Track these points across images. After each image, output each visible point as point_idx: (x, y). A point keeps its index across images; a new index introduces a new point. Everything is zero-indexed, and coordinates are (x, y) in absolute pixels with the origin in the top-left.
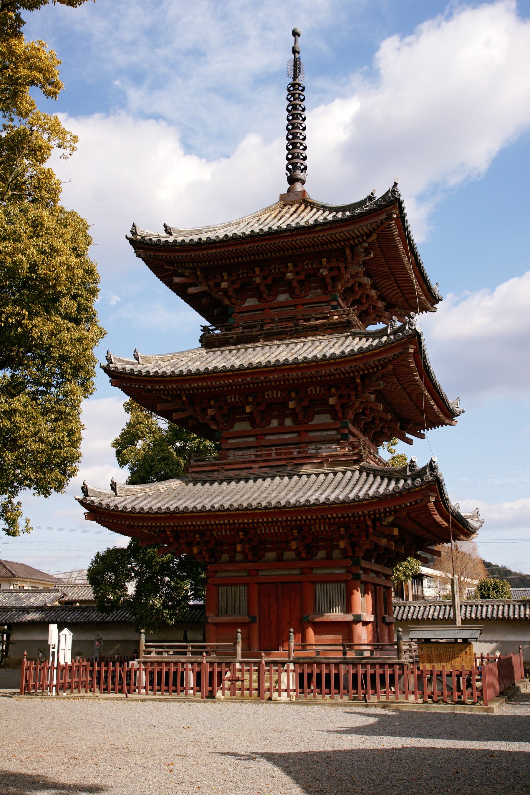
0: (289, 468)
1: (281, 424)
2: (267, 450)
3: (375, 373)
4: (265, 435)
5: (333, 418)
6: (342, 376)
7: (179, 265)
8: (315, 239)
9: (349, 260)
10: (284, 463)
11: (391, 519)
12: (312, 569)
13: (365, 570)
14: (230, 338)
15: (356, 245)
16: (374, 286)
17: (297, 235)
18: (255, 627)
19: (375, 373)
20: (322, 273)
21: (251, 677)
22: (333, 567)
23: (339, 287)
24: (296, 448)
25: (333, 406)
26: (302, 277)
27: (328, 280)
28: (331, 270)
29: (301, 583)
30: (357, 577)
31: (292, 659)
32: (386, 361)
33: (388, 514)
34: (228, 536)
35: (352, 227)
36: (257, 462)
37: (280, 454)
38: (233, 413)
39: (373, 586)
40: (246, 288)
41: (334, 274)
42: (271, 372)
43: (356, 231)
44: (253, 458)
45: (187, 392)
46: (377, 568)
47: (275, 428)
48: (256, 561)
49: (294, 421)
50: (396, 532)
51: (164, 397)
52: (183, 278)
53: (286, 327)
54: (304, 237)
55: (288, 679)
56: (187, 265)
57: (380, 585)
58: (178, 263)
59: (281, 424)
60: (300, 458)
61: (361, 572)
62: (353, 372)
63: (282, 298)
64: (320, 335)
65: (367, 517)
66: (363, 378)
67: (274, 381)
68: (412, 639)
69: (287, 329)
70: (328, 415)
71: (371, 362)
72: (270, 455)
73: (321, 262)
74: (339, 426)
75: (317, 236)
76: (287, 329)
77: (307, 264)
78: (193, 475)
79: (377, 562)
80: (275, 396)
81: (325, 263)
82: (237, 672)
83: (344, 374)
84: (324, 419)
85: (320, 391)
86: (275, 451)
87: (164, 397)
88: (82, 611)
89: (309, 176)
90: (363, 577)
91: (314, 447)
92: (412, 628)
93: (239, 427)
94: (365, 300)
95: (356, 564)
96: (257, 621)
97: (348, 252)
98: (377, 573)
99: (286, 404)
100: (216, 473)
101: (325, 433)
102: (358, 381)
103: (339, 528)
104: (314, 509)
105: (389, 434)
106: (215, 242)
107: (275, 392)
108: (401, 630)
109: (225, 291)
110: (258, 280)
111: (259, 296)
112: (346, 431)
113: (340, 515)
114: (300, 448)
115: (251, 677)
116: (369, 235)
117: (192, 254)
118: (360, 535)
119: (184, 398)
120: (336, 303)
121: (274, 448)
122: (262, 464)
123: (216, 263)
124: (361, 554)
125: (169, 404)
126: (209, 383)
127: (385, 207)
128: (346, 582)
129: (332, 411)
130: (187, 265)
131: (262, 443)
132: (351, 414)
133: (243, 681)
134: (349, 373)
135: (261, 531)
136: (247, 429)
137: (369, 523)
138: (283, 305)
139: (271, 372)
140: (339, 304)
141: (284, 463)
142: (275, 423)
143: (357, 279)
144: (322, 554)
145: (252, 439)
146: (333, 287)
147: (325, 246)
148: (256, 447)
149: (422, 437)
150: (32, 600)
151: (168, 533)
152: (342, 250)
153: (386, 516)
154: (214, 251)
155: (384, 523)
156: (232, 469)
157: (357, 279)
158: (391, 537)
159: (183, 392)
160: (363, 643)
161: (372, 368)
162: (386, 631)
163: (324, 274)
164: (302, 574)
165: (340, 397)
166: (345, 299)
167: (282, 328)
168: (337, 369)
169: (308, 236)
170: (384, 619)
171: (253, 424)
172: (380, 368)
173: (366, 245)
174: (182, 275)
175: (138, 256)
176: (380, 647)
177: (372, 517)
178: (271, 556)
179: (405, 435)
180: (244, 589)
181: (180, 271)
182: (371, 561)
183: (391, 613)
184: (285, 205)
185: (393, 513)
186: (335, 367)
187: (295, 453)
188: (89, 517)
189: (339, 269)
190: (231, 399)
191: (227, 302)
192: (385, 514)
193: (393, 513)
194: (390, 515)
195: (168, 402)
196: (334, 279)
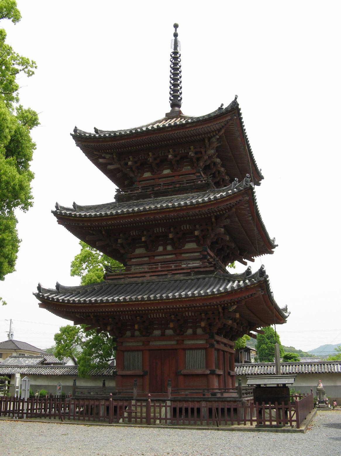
0: (169, 276)
1: (165, 249)
2: (155, 265)
3: (224, 214)
4: (154, 256)
5: (197, 245)
6: (203, 216)
7: (103, 151)
8: (186, 133)
9: (207, 146)
10: (166, 273)
11: (235, 307)
12: (183, 341)
13: (218, 342)
14: (133, 196)
15: (212, 137)
16: (223, 166)
17: (175, 130)
18: (147, 378)
19: (224, 214)
20: (191, 155)
21: (141, 410)
22: (197, 339)
23: (202, 164)
24: (174, 263)
25: (197, 236)
26: (178, 158)
27: (194, 160)
28: (196, 153)
29: (176, 349)
30: (212, 346)
31: (169, 398)
32: (231, 205)
33: (232, 304)
34: (129, 320)
35: (209, 125)
36: (149, 272)
37: (164, 267)
38: (134, 242)
39: (222, 352)
40: (143, 166)
41: (199, 156)
42: (158, 213)
43: (211, 127)
44: (146, 270)
45: (105, 228)
46: (225, 341)
47: (160, 252)
48: (148, 336)
49: (173, 247)
50: (238, 316)
51: (91, 232)
52: (105, 160)
53: (168, 189)
54: (179, 131)
55: (165, 411)
56: (107, 151)
57: (226, 352)
58: (100, 148)
59: (165, 249)
60: (176, 270)
61: (215, 343)
62: (210, 213)
63: (166, 172)
64: (189, 193)
65: (219, 306)
66: (217, 218)
67: (160, 220)
68: (249, 385)
69: (169, 190)
70: (194, 243)
71: (222, 206)
72: (157, 268)
73: (190, 149)
74: (201, 250)
75: (187, 130)
76: (169, 190)
77: (182, 150)
78: (108, 281)
79: (225, 337)
80: (161, 231)
81: (192, 149)
82: (132, 407)
83: (204, 214)
84: (192, 245)
85: (189, 227)
86: (160, 266)
87: (91, 232)
88: (51, 368)
89: (183, 103)
90: (217, 346)
91: (185, 263)
92: (249, 377)
93: (138, 251)
94: (217, 175)
95: (212, 337)
96: (148, 374)
97: (207, 141)
98: (225, 345)
99: (168, 236)
100: (123, 280)
101: (192, 254)
102: (213, 220)
103: (201, 314)
104: (185, 300)
105: (232, 258)
106: (124, 135)
107: (160, 228)
108: (241, 379)
109: (131, 168)
110: (151, 160)
111: (152, 171)
112: (206, 253)
113: (201, 304)
114: (176, 263)
115: (141, 410)
116: (219, 130)
117: (110, 143)
118: (214, 319)
119: (104, 233)
120: (199, 174)
121: (159, 264)
122: (152, 274)
123: (125, 149)
124: (215, 331)
125: (94, 236)
126: (118, 221)
127: (230, 112)
128: (206, 349)
129: (197, 240)
130: (107, 151)
131: (152, 261)
132: (209, 242)
133: (136, 413)
134: (207, 214)
135: (151, 316)
136: (143, 252)
137: (220, 310)
138: (166, 176)
139: (158, 213)
140: (201, 174)
141: (166, 273)
142: (161, 249)
143: (212, 160)
144: (190, 331)
145: (147, 259)
146: (198, 164)
147: (192, 138)
148: (149, 264)
149: (253, 261)
150: (27, 362)
151: (92, 317)
152: (203, 140)
153: (231, 306)
154: (124, 141)
155: (230, 310)
156: (133, 277)
157: (212, 160)
158: (234, 320)
159: (102, 228)
160: (215, 388)
161: (222, 210)
162: (230, 381)
163: (192, 155)
164: (177, 344)
165: (202, 231)
166: (205, 173)
167: (165, 189)
168: (199, 211)
169: (182, 131)
170: (229, 373)
171: (147, 249)
172: (227, 211)
173: (218, 137)
174: (104, 158)
175: (78, 145)
176: (227, 391)
177: (223, 306)
178: (157, 333)
179: (242, 259)
180: (140, 353)
181: (103, 155)
182: (221, 336)
183: (233, 370)
184: (169, 119)
185: (236, 303)
186: (198, 210)
187: (173, 267)
188: (41, 306)
189: (201, 153)
190: (133, 233)
191: (132, 175)
192: (231, 304)
193: (236, 303)
194: (234, 304)
195: (94, 235)
196: (198, 159)
